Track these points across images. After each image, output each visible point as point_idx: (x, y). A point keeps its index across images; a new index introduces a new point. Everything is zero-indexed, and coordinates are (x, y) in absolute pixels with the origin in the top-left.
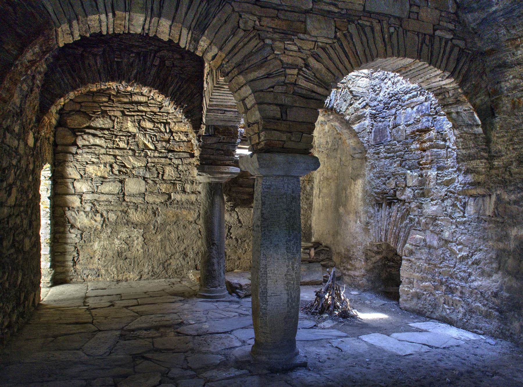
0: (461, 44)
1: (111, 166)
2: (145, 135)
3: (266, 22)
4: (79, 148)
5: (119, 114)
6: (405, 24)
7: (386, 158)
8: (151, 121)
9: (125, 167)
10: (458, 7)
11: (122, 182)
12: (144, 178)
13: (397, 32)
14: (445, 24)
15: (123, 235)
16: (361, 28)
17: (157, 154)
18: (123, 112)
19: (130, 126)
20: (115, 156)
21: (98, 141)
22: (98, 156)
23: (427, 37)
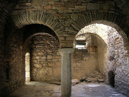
0: (118, 14)
1: (44, 52)
2: (52, 44)
3: (60, 17)
4: (36, 48)
5: (45, 40)
6: (99, 11)
7: (111, 47)
8: (53, 41)
9: (47, 52)
10: (116, 4)
11: (47, 56)
12: (52, 55)
13: (97, 14)
14: (112, 9)
15: (47, 69)
16: (86, 14)
17: (55, 49)
18: (46, 39)
19: (48, 42)
20: (45, 50)
21: (40, 46)
22: (41, 50)
23: (106, 14)
